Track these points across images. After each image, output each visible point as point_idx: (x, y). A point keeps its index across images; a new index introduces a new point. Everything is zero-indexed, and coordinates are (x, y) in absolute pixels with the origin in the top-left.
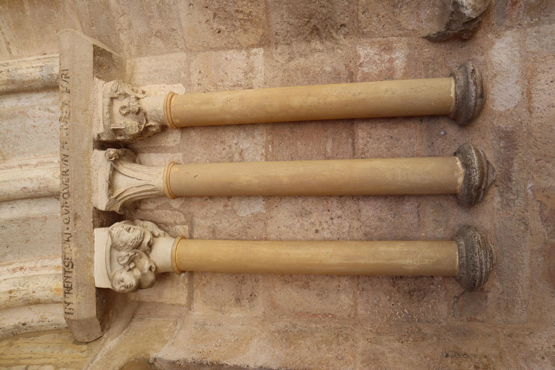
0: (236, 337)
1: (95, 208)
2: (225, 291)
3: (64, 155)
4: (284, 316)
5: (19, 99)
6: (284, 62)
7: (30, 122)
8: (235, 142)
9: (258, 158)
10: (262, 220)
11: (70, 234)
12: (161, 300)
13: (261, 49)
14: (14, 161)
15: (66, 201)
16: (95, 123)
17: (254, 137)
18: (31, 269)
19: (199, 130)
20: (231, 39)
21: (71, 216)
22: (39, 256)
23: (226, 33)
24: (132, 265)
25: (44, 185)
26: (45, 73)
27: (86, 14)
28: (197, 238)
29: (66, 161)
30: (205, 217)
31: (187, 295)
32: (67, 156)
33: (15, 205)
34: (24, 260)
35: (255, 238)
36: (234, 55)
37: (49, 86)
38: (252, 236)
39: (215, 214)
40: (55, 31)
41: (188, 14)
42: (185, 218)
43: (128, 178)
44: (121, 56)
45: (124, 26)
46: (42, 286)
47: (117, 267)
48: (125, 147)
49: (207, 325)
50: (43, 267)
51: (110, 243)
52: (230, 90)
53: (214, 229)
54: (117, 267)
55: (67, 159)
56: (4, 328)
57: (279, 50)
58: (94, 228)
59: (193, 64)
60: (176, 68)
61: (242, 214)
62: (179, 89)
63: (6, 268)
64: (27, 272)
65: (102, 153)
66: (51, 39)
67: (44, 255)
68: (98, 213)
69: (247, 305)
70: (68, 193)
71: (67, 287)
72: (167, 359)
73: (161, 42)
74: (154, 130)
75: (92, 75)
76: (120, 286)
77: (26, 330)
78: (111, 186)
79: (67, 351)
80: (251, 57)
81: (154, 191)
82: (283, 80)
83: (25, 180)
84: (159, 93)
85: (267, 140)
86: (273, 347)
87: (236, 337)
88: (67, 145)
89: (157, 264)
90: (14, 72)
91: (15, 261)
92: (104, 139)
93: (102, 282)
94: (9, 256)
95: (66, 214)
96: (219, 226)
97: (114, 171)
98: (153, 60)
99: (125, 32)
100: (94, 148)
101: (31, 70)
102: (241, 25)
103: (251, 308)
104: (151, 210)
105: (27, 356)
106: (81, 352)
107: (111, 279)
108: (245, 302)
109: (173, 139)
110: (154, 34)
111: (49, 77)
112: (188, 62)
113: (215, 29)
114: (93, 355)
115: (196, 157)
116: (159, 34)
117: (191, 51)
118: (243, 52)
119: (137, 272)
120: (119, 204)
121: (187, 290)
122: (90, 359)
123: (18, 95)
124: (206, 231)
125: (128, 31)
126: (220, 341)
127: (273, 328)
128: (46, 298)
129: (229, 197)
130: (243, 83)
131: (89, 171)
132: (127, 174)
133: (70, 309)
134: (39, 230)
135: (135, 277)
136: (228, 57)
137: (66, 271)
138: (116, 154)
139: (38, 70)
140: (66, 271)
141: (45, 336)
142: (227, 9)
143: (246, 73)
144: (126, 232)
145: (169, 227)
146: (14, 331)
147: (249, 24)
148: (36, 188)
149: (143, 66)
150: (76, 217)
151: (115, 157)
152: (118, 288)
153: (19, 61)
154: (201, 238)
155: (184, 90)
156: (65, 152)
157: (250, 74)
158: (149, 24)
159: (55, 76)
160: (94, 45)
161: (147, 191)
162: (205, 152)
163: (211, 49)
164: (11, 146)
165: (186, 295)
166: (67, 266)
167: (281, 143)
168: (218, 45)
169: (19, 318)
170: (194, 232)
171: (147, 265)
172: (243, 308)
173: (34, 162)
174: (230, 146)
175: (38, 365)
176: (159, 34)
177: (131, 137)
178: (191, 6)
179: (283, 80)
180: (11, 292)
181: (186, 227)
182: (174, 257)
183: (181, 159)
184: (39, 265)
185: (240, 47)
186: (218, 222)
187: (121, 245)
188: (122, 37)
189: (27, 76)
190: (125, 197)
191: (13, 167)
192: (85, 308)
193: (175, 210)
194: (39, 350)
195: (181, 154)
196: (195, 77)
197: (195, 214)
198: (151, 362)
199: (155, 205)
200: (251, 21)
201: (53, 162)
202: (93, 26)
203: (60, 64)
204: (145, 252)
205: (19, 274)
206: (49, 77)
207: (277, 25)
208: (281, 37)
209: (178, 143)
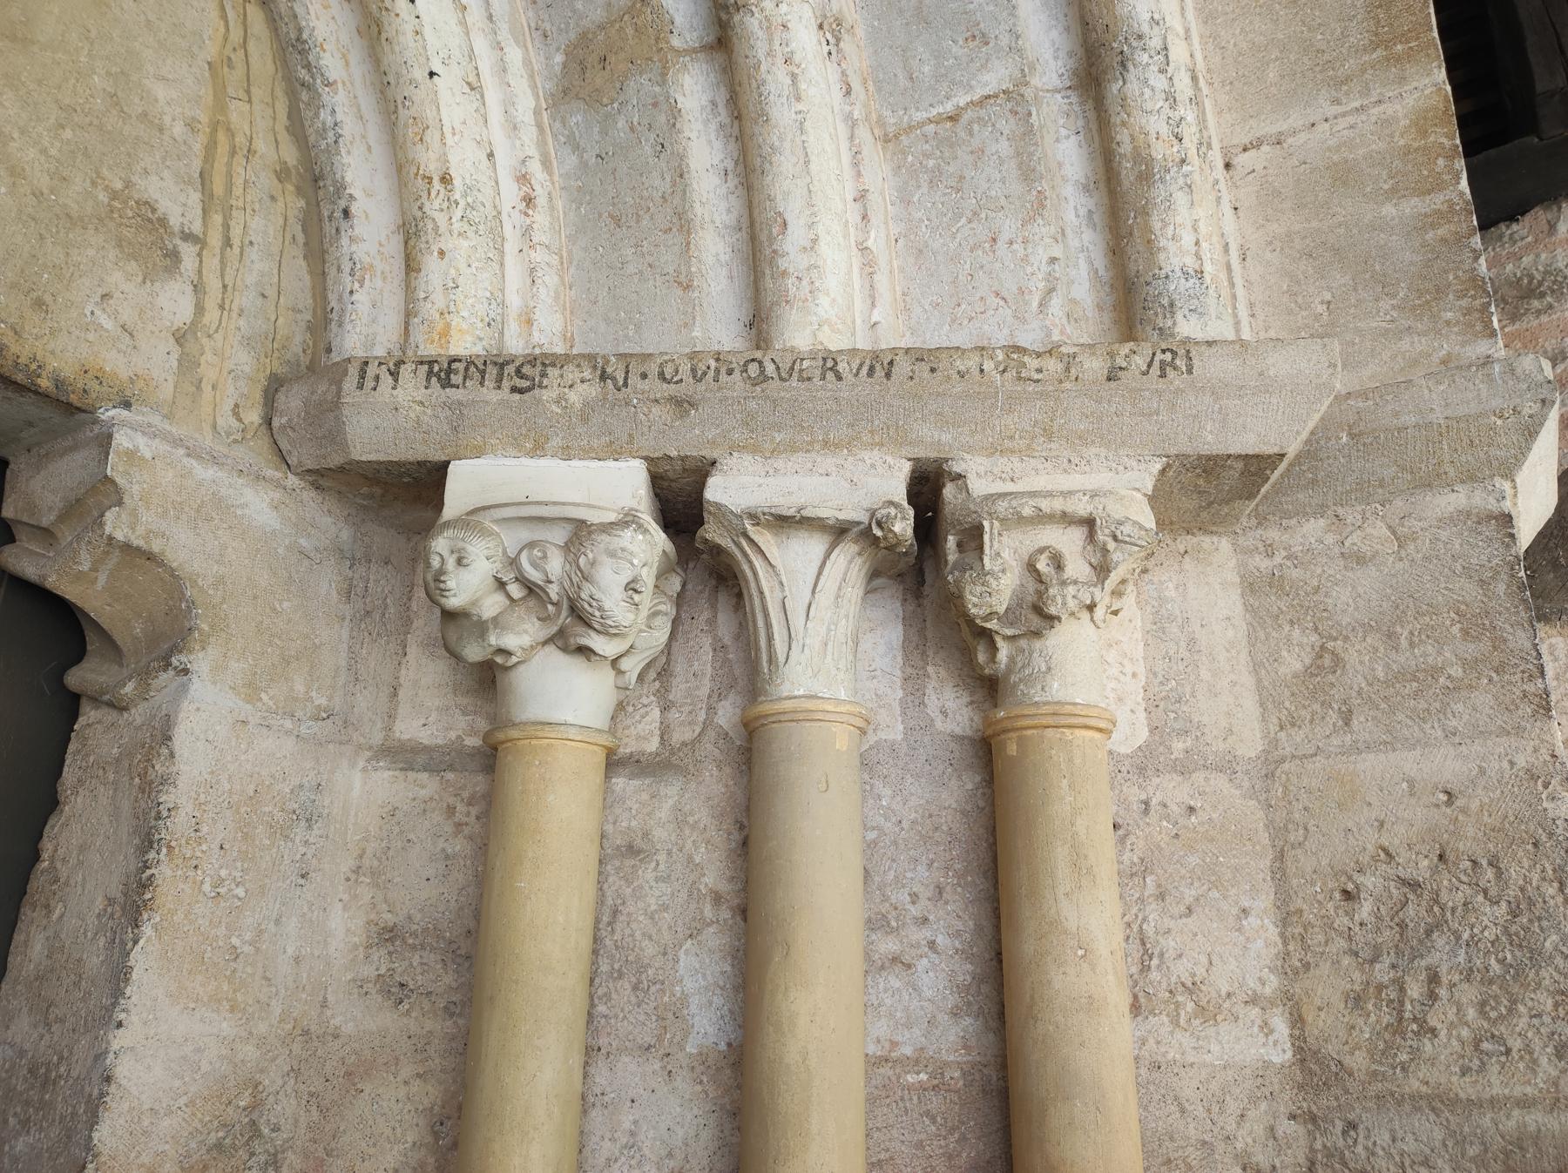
0: (247, 949)
1: (714, 463)
2: (422, 890)
3: (891, 363)
4: (315, 1113)
5: (1086, 189)
6: (1239, 1145)
7: (1008, 226)
8: (940, 940)
9: (882, 1029)
10: (660, 1039)
11: (626, 384)
12: (413, 650)
13: (1289, 1054)
14: (879, 173)
15: (737, 374)
16: (1003, 463)
17: (955, 1014)
18: (527, 232)
19: (981, 804)
20: (1321, 938)
21: (687, 388)
22: (570, 252)
23: (1346, 920)
24: (516, 591)
25: (792, 291)
26: (1179, 286)
27: (1396, 414)
28: (607, 790)
29: (872, 370)
30: (680, 819)
31: (426, 742)
32: (888, 375)
33: (733, 181)
34: (559, 204)
35: (601, 1009)
36: (1260, 943)
37: (1132, 300)
38: (608, 996)
39: (690, 859)
40: (1328, 297)
41: (1411, 783)
42: (684, 744)
43: (815, 571)
44: (1244, 520)
45: (1356, 538)
46: (461, 281)
47: (513, 538)
48: (923, 555)
49: (310, 827)
50: (533, 270)
51: (594, 517)
52: (1129, 925)
53: (639, 852)
54: (513, 538)
55: (879, 373)
56: (339, 153)
57: (1286, 1127)
58: (646, 458)
59: (1220, 782)
60: (1205, 720)
61: (687, 960)
62: (1131, 733)
63: (532, 151)
64: (517, 218)
65: (899, 493)
66: (1298, 282)
67: (572, 270)
68: (702, 471)
69: (369, 971)
70: (763, 378)
71: (449, 371)
72: (182, 715)
73: (1298, 666)
74: (981, 657)
75: (1173, 451)
76: (446, 554)
77: (330, 218)
78: (784, 522)
79: (243, 360)
80: (1255, 1012)
81: (770, 661)
82: (1172, 1139)
83: (811, 226)
84: (1111, 656)
85: (946, 1064)
86: (191, 1103)
87: (247, 949)
88: (926, 374)
89: (521, 668)
90: (1181, 181)
91: (556, 178)
92: (949, 491)
93: (466, 484)
94: (572, 160)
95: (694, 370)
96: (647, 874)
97: (839, 531)
98: (1230, 633)
99: (1330, 539)
100: (916, 460)
101: (1188, 239)
102: (1380, 988)
103: (360, 984)
104: (712, 622)
105: (236, 232)
106: (237, 406)
107: (471, 520)
108: (380, 962)
109: (951, 709)
110: (1330, 645)
111: (1165, 302)
112: (1227, 766)
113: (1360, 879)
114: (221, 449)
115: (887, 792)
116: (1327, 661)
117: (1269, 776)
118: (1273, 982)
119: (492, 605)
120: (725, 542)
121: (440, 742)
122: (208, 440)
123: (1102, 185)
124: (634, 823)
125: (1336, 550)
126: (240, 892)
127: (271, 1080)
128: (422, 295)
129: (743, 912)
130: (1154, 975)
131: (837, 446)
132: (825, 572)
133: (377, 378)
134: (649, 259)
135: (474, 603)
136: (1252, 922)
137: (502, 366)
138: (894, 541)
139: (1190, 262)
140: (502, 366)
141: (307, 278)
142: (1440, 940)
143: (1192, 989)
144: (625, 578)
145: (657, 684)
146: (329, 182)
147: (1386, 1019)
148: (783, 263)
149: (1209, 585)
150: (682, 405)
151: (885, 538)
152: (440, 544)
153: (1217, 182)
154: (608, 800)
155: (1124, 750)
156: (903, 367)
157: (1190, 1006)
158: (1368, 628)
159: (1170, 323)
160: (1283, 455)
161: (770, 638)
162: (905, 824)
163: (1281, 856)
164: (931, 163)
165: (426, 737)
166: (518, 371)
167: (933, 1120)
168: (1295, 882)
169: (369, 195)
170: (632, 776)
171: (511, 641)
172: (361, 952)
173: (876, 240)
174: (926, 920)
175: (200, 272)
176: (1327, 661)
177: (953, 589)
178: (1444, 797)
179: (1172, 1139)
180: (446, 179)
181: (653, 745)
182: (540, 734)
183: (882, 735)
184: (539, 256)
185: (1295, 965)
186: (662, 867)
187: (582, 561)
188: (1313, 529)
189: (1165, 225)
190: (750, 562)
191: (859, 174)
192: (383, 425)
193: (711, 710)
194: (256, 267)
195: (900, 737)
196: (1171, 790)
197: (693, 785)
198: (174, 661)
199: (727, 640)
200: (1398, 1028)
201: (873, 305)
202: (1352, 436)
203: (1209, 344)
204: (561, 633)
205: (511, 194)
206: (1165, 302)
207: (1387, 1137)
208: (1341, 1143)
209: (939, 724)
